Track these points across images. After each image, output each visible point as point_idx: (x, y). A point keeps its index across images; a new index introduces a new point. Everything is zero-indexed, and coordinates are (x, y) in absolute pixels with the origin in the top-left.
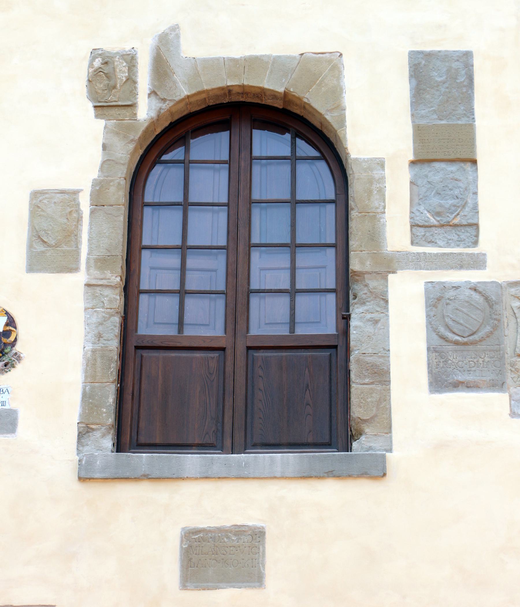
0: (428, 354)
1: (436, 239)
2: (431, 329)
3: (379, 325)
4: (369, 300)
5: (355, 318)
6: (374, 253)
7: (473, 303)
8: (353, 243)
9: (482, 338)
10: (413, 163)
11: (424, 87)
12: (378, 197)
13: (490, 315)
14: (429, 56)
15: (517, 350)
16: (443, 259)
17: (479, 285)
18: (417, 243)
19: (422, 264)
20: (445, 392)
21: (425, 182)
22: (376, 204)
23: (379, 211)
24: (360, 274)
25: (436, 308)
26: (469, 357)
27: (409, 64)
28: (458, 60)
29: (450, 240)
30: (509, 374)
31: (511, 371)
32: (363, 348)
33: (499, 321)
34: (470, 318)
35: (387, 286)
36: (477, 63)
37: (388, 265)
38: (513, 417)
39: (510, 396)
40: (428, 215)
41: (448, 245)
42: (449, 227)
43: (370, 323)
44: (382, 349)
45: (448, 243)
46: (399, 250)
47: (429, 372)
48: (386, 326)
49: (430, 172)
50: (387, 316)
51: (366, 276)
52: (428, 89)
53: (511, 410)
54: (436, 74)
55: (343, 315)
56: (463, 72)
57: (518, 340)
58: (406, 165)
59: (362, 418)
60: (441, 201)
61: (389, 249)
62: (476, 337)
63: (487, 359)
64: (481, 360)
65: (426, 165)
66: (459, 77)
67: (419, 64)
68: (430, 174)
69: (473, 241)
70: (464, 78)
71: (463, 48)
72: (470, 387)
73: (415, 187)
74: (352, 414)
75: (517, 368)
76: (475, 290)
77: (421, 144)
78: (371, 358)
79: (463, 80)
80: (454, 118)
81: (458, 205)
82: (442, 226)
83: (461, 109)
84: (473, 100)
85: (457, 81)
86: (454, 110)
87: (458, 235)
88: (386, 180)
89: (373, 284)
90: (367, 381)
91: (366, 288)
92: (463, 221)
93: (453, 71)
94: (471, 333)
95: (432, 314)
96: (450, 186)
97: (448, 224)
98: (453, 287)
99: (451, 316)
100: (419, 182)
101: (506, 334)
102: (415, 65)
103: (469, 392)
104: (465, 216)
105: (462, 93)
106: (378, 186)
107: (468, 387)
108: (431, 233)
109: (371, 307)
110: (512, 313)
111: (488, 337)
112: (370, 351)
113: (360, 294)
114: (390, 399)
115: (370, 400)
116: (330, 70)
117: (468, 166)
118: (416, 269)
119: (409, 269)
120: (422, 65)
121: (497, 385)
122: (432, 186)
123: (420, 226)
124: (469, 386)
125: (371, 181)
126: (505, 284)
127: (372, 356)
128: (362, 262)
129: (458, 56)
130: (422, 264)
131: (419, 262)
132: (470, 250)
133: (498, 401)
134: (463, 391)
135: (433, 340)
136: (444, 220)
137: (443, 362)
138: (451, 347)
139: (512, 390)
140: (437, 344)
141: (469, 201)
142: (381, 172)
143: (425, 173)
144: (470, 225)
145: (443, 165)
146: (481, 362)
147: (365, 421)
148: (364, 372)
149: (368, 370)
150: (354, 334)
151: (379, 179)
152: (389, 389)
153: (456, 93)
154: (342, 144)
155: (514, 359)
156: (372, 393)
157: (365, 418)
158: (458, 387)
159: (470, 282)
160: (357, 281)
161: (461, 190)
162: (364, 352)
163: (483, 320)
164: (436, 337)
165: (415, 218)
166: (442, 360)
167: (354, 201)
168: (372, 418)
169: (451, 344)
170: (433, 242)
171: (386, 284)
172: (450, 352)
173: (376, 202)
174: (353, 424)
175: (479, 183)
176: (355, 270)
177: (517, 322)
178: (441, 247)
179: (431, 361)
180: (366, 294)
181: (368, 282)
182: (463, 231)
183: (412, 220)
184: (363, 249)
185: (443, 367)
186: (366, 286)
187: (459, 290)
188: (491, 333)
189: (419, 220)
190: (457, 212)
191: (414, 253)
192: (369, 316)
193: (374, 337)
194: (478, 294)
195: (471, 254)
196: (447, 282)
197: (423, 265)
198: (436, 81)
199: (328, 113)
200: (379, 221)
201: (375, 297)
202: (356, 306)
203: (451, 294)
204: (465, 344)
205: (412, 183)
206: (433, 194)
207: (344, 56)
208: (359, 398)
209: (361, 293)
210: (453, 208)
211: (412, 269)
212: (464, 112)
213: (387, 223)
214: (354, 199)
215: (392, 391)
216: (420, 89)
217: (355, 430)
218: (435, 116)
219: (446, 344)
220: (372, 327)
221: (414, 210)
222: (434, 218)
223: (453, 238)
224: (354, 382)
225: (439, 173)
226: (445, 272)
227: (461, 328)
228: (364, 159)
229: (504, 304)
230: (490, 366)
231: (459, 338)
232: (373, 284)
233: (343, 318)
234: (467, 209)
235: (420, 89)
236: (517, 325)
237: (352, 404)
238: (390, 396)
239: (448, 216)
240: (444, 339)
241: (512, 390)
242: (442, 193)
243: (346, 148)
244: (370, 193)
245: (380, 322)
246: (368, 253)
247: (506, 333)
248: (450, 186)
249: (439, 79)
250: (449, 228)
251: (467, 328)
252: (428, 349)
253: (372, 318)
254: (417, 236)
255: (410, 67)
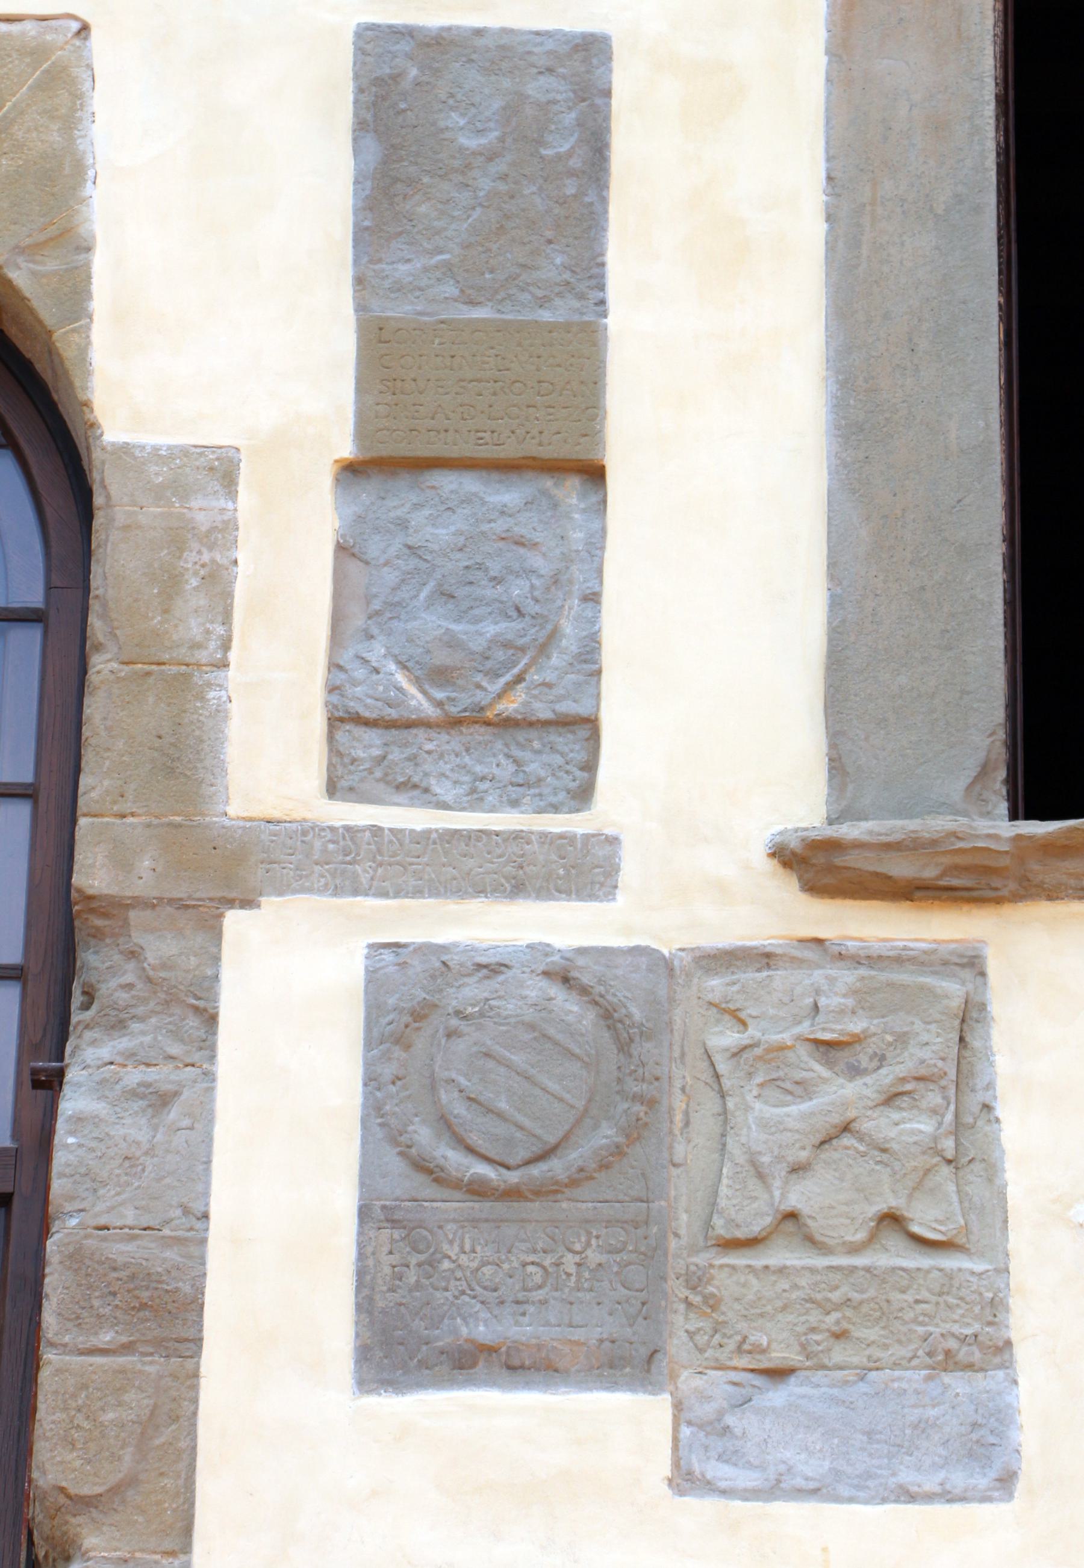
0: (360, 1233)
1: (426, 774)
2: (380, 1133)
3: (173, 1114)
4: (140, 1010)
5: (79, 1085)
6: (170, 824)
7: (551, 1032)
8: (93, 785)
9: (581, 1170)
10: (352, 471)
11: (412, 169)
12: (202, 602)
13: (619, 1080)
14: (437, 46)
15: (718, 1222)
16: (446, 853)
17: (581, 962)
18: (351, 789)
19: (363, 872)
20: (421, 1385)
21: (396, 546)
22: (194, 628)
23: (203, 656)
24: (113, 908)
25: (407, 1047)
26: (523, 1246)
27: (356, 77)
28: (550, 70)
29: (483, 779)
30: (679, 1320)
31: (689, 1304)
32: (100, 1207)
33: (652, 1103)
34: (537, 1092)
35: (217, 959)
36: (626, 81)
37: (230, 871)
38: (681, 1492)
39: (678, 1407)
40: (401, 678)
41: (475, 800)
42: (483, 729)
43: (138, 1105)
44: (178, 1212)
45: (473, 791)
46: (276, 814)
47: (359, 1307)
48: (203, 1117)
49: (417, 506)
50: (210, 1077)
51: (132, 914)
52: (426, 180)
53: (676, 1463)
54: (462, 122)
55: (35, 1072)
56: (569, 118)
57: (725, 1181)
58: (326, 480)
59: (72, 1491)
60: (453, 627)
61: (232, 811)
62: (556, 1167)
63: (594, 1257)
64: (570, 1260)
65: (403, 481)
66: (549, 138)
67: (396, 78)
68: (418, 518)
69: (573, 785)
70: (573, 140)
71: (574, 20)
72: (522, 1367)
73: (354, 567)
74: (35, 1475)
75: (713, 1295)
76: (566, 980)
77: (389, 398)
78: (130, 1247)
79: (565, 147)
80: (525, 297)
81: (520, 642)
82: (454, 723)
83: (554, 264)
84: (604, 230)
85: (543, 152)
86: (524, 266)
87: (516, 761)
88: (241, 535)
89: (160, 947)
90: (106, 1337)
91: (131, 965)
92: (537, 705)
93: (529, 111)
94: (537, 1149)
95: (388, 1071)
96: (495, 567)
97: (475, 718)
98: (480, 966)
99: (462, 1081)
100: (374, 548)
101: (678, 1157)
102: (378, 81)
103: (514, 1386)
104: (549, 686)
105: (562, 202)
106: (206, 557)
107: (511, 1368)
108: (409, 751)
109: (148, 1039)
110: (707, 1076)
111: (604, 1166)
112: (130, 1216)
113: (110, 989)
114: (195, 1414)
115: (111, 1415)
116: (39, 86)
117: (570, 492)
118: (337, 892)
119: (309, 890)
120: (406, 84)
121: (628, 1364)
122: (424, 566)
123: (367, 723)
124: (516, 1362)
125: (178, 536)
126: (687, 958)
127: (134, 1238)
128: (122, 862)
129: (549, 53)
130: (363, 872)
131: (347, 865)
132: (556, 823)
133: (626, 1426)
134: (490, 1382)
135: (384, 1176)
136: (463, 701)
137: (419, 1265)
138: (456, 1206)
139: (688, 1381)
140: (398, 1192)
141: (567, 627)
142: (222, 503)
143: (399, 513)
144: (565, 723)
145: (469, 483)
146: (572, 1269)
147: (87, 1503)
148: (96, 1303)
149: (114, 1294)
150: (67, 1144)
151: (213, 529)
152: (196, 1375)
153: (538, 200)
154: (71, 384)
155: (701, 1259)
156: (122, 1390)
157: (86, 1490)
158: (474, 1365)
159: (545, 950)
160: (98, 934)
161: (537, 582)
162: (102, 1221)
163: (590, 1100)
164: (395, 1164)
165: (349, 691)
166: (414, 1260)
167: (104, 616)
168: (116, 1490)
169: (458, 1195)
170: (415, 786)
171: (215, 950)
172: (450, 1227)
173: (193, 623)
174: (39, 1518)
175: (607, 555)
176: (90, 892)
177: (725, 1112)
178: (444, 806)
179: (371, 1262)
180: (130, 986)
181: (141, 942)
182: (536, 745)
183: (335, 698)
184: (127, 806)
185: (418, 1286)
186: (133, 954)
187: (501, 978)
188: (619, 1151)
189: (362, 698)
190: (516, 671)
191: (332, 829)
192: (134, 1076)
193: (149, 1161)
194: (574, 996)
195: (562, 836)
196: (455, 945)
197: (364, 879)
198: (461, 149)
199: (20, 260)
200: (203, 699)
201: (167, 1003)
202: (88, 1035)
203: (471, 992)
204: (512, 1194)
205: (343, 550)
206: (423, 595)
207: (96, 35)
208: (66, 1409)
209: (113, 983)
210: (500, 655)
211: (322, 891)
212: (567, 276)
213: (234, 708)
214: (105, 606)
215: (203, 1382)
216: (396, 180)
217: (47, 1539)
218: (450, 289)
219: (438, 1196)
220: (143, 1121)
221: (346, 657)
222: (424, 693)
223: (496, 771)
224: (52, 1345)
225: (448, 513)
226: (452, 907)
227: (501, 1129)
228: (156, 449)
229: (677, 1037)
230: (606, 1284)
231: (482, 1169)
232: (160, 947)
233: (37, 1084)
234: (555, 660)
235: (396, 180)
236: (726, 1121)
237: (38, 1431)
238: (195, 1401)
239: (479, 686)
240: (430, 1172)
241: (688, 1381)
242: (461, 592)
243: (87, 404)
244: (171, 584)
245: (177, 1100)
246: (149, 826)
247: (680, 1150)
248: (495, 567)
249: (471, 142)
250: (480, 734)
251: (521, 1128)
252: (364, 1213)
253: (148, 1085)
254: (353, 761)
255: (360, 90)
